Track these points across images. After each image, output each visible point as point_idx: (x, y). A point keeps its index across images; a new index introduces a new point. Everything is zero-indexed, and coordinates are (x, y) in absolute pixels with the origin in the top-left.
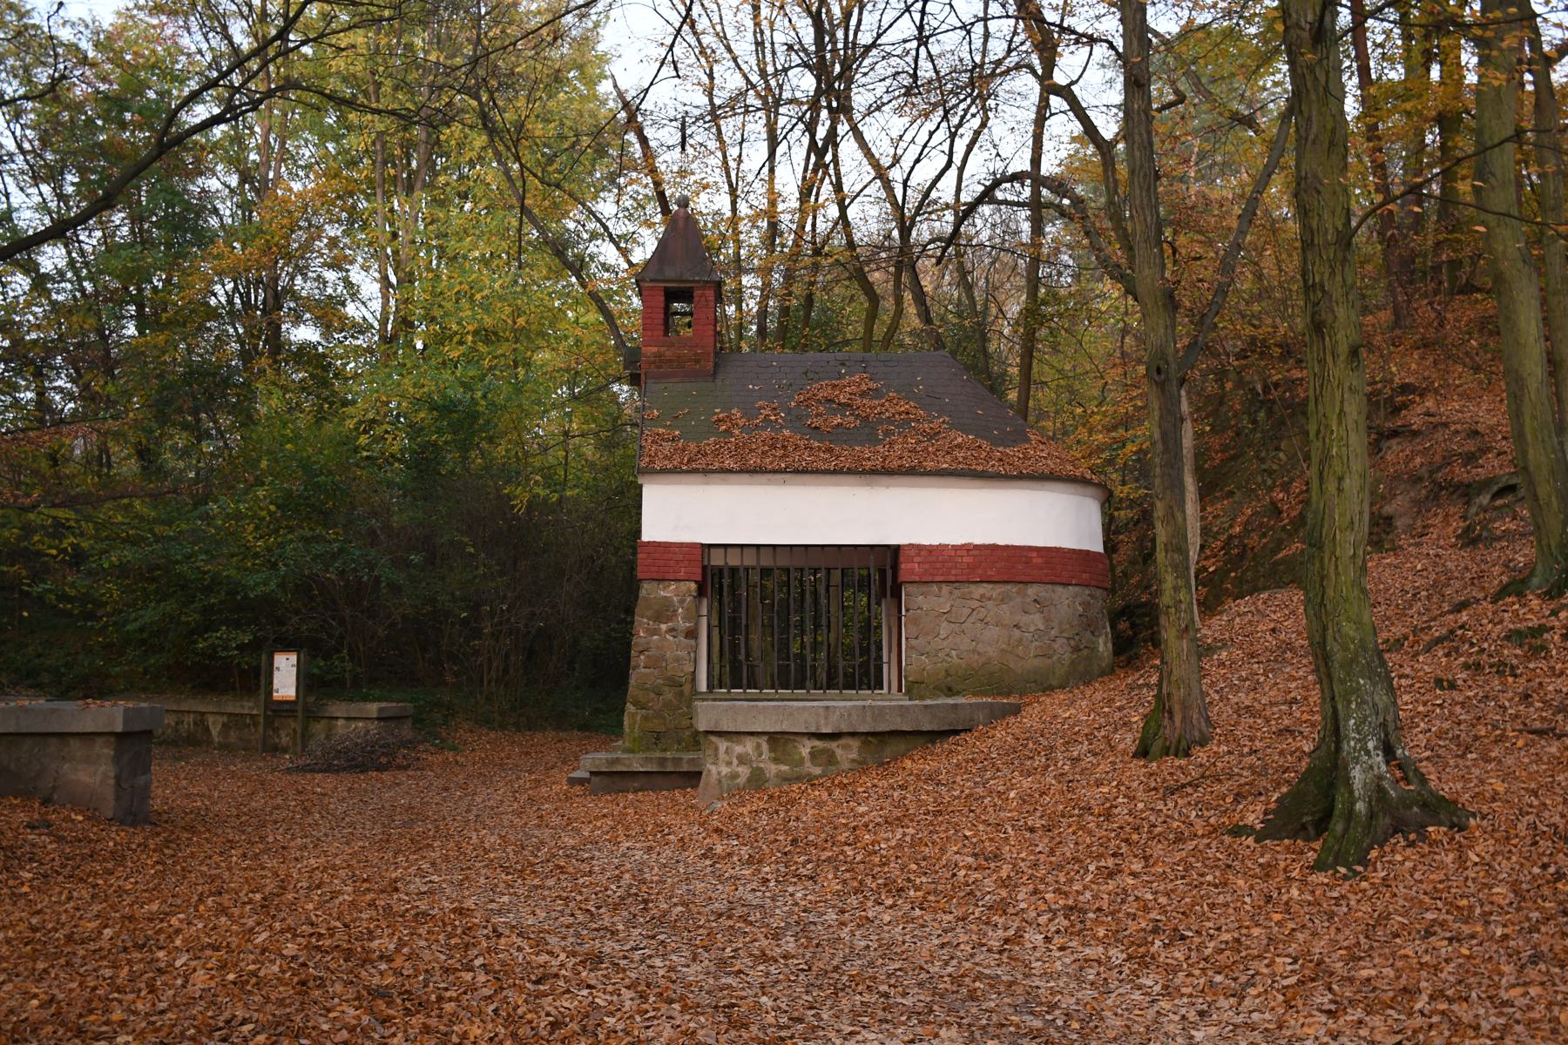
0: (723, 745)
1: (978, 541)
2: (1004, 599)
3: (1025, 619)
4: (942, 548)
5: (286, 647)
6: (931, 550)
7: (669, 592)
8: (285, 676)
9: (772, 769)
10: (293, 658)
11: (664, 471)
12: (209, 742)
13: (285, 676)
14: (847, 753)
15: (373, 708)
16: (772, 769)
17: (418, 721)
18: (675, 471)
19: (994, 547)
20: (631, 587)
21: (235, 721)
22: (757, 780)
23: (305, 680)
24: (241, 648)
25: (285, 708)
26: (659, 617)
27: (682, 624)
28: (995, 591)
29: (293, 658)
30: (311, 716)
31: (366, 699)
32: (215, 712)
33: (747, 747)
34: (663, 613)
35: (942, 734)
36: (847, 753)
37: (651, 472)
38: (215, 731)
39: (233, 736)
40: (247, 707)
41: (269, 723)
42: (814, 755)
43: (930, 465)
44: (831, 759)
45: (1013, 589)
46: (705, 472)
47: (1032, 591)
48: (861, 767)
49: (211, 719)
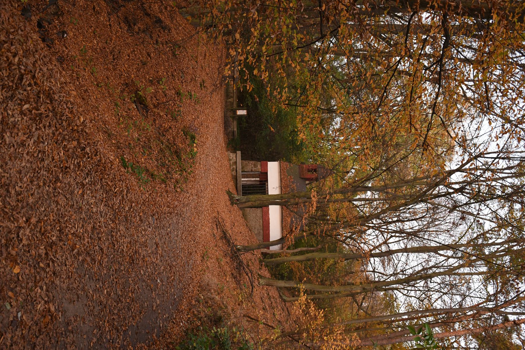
0: (235, 155)
1: (270, 221)
2: (260, 226)
3: (256, 230)
4: (269, 214)
5: (247, 112)
6: (268, 212)
7: (259, 167)
8: (242, 112)
9: (231, 162)
10: (246, 114)
11: (280, 165)
12: (227, 99)
13: (242, 112)
14: (234, 173)
15: (236, 129)
16: (231, 162)
17: (233, 140)
18: (280, 167)
19: (269, 224)
20: (259, 160)
21: (232, 104)
22: (230, 160)
23: (241, 116)
24: (248, 104)
25: (235, 113)
26: (254, 165)
27: (253, 169)
28: (261, 224)
29: (246, 114)
30: (234, 118)
31: (237, 129)
32: (234, 100)
33: (235, 158)
34: (255, 166)
35: (237, 189)
36: (234, 173)
37: (280, 163)
38: (230, 100)
39: (229, 104)
40: (235, 105)
41: (232, 110)
42: (234, 168)
43: (284, 211)
44: (233, 171)
45: (262, 228)
46: (280, 172)
47: (261, 231)
48: (232, 175)
49: (232, 99)
